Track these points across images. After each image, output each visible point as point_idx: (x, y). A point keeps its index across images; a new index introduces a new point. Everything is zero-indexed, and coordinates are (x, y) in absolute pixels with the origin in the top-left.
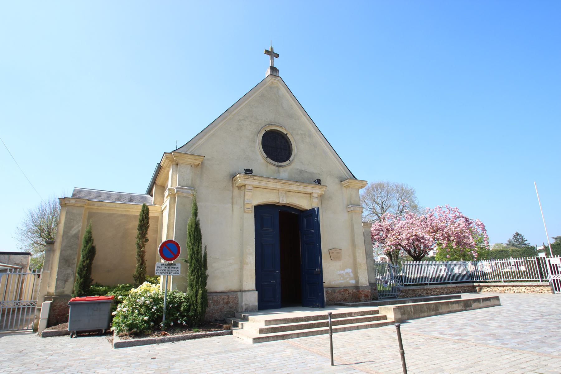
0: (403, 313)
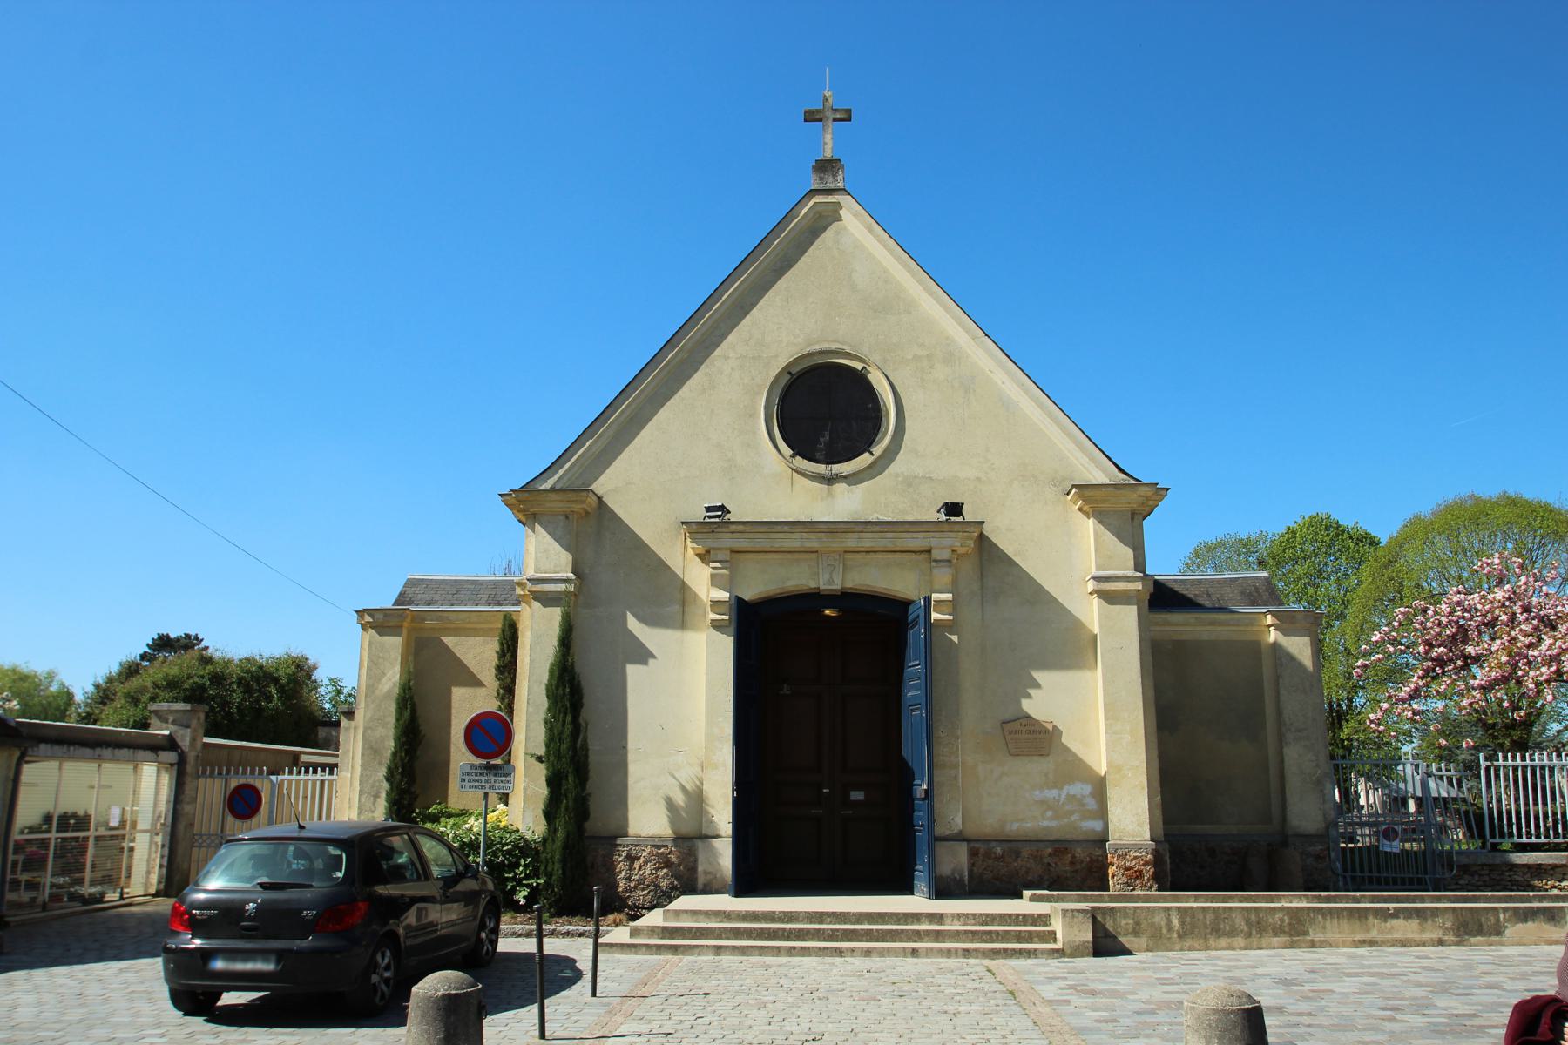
0: (1130, 930)
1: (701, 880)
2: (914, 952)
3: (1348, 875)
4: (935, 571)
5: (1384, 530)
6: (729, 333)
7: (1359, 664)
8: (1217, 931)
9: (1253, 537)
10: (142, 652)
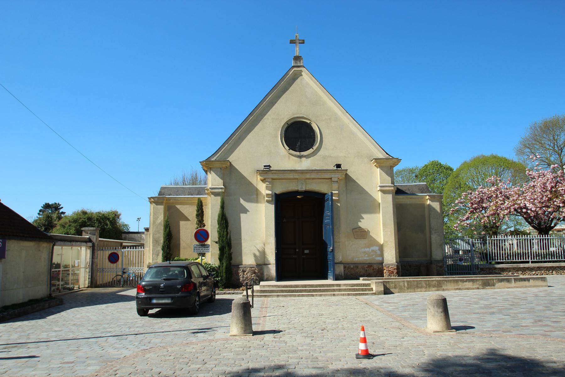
0: (394, 287)
1: (265, 277)
2: (334, 295)
5: (455, 166)
6: (269, 111)
7: (451, 210)
9: (414, 168)
10: (40, 209)
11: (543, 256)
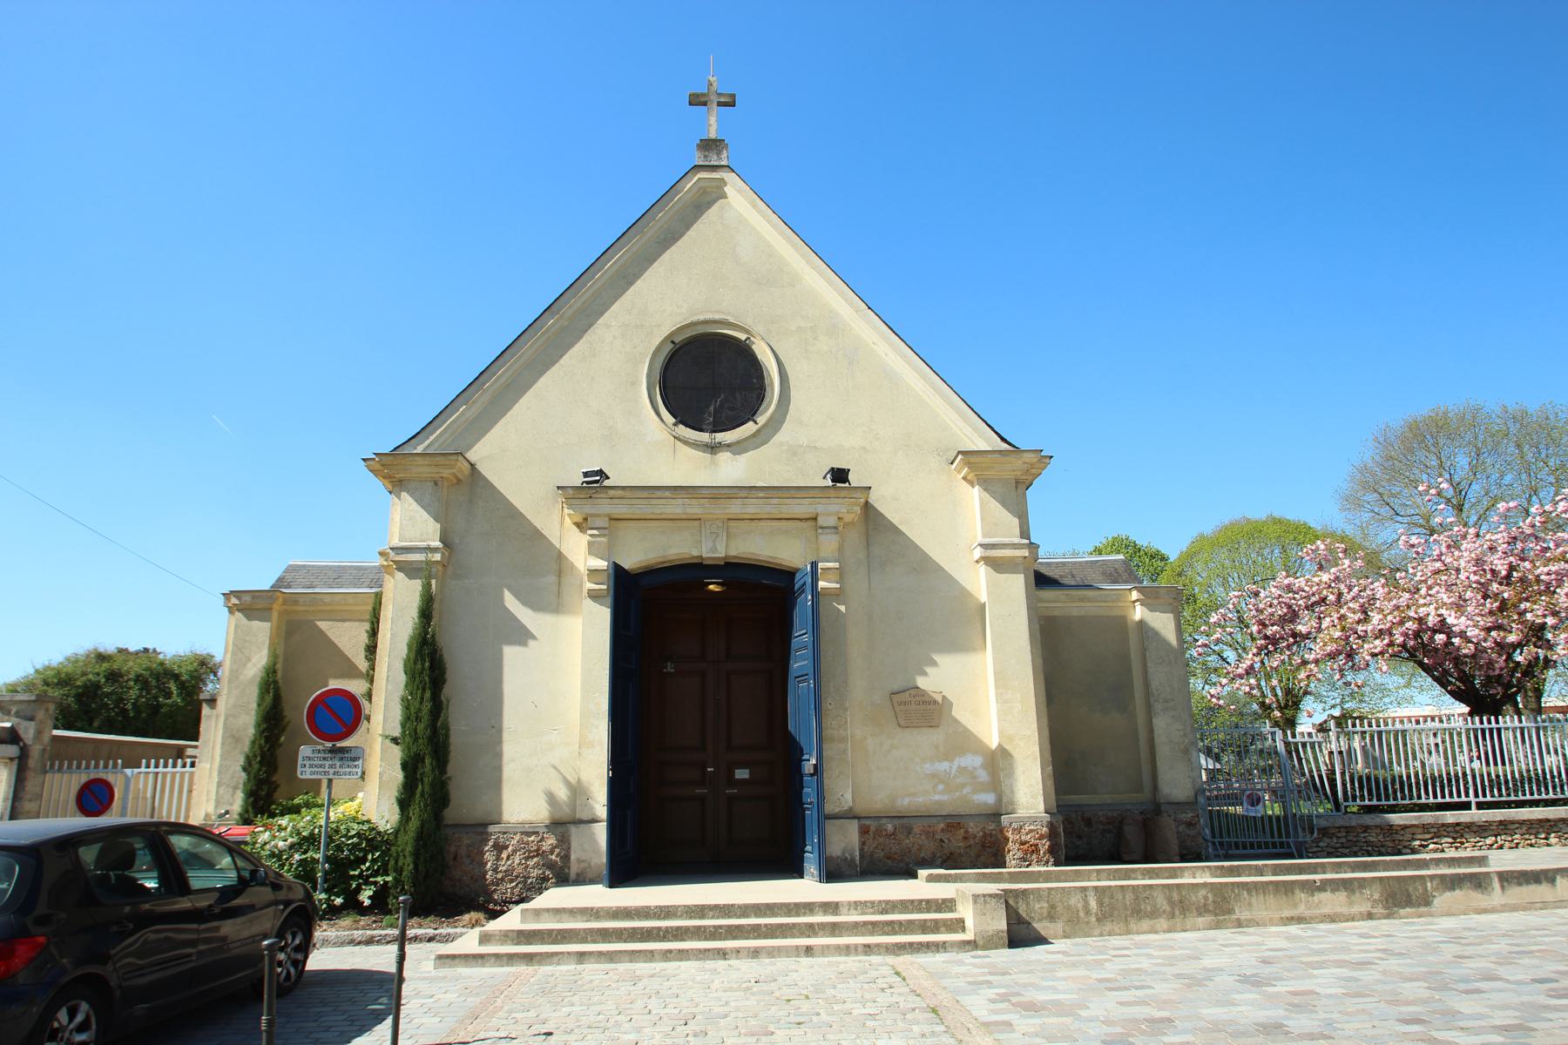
0: (1045, 914)
1: (574, 869)
2: (809, 950)
3: (1217, 840)
4: (822, 538)
8: (1138, 913)
11: (1511, 786)
